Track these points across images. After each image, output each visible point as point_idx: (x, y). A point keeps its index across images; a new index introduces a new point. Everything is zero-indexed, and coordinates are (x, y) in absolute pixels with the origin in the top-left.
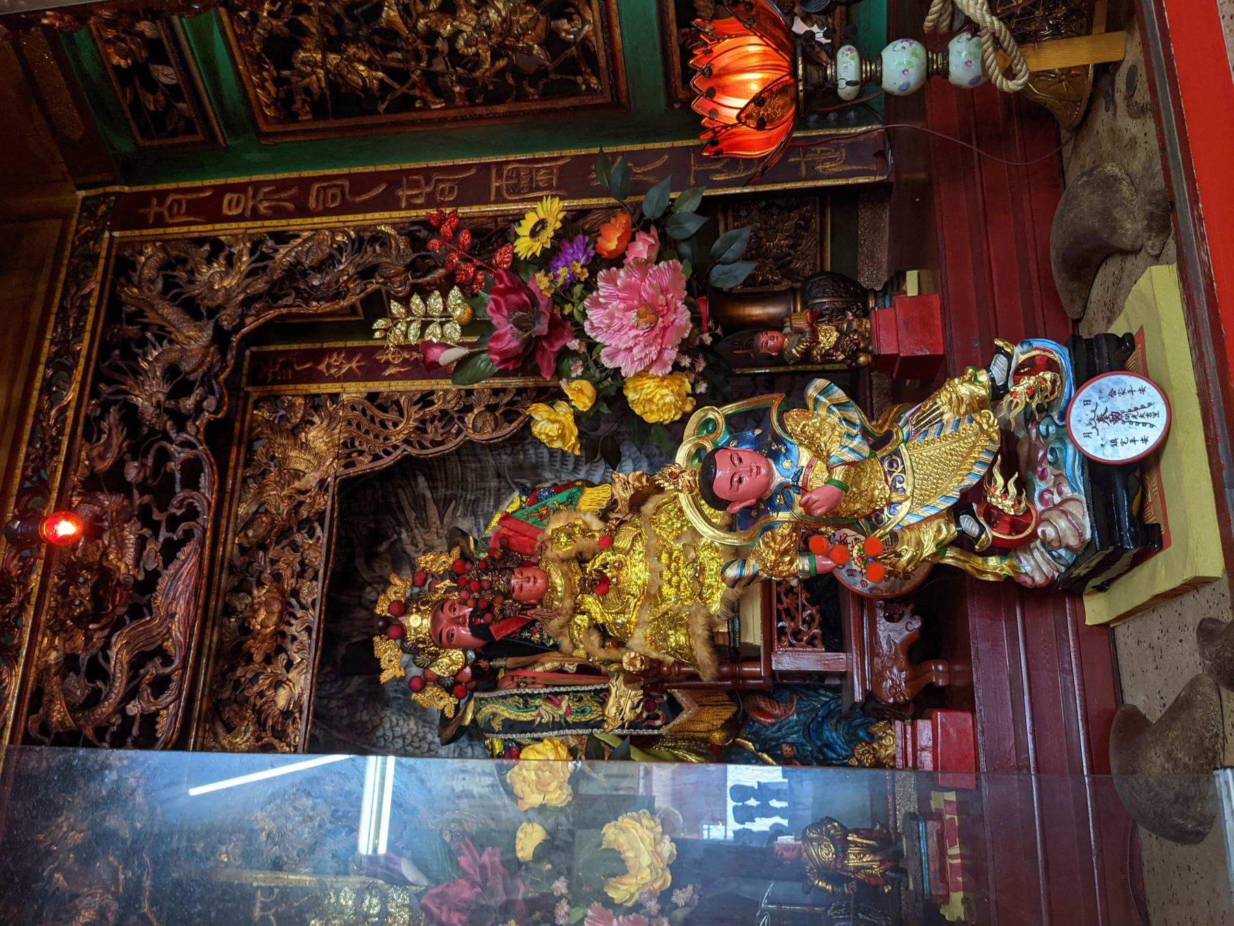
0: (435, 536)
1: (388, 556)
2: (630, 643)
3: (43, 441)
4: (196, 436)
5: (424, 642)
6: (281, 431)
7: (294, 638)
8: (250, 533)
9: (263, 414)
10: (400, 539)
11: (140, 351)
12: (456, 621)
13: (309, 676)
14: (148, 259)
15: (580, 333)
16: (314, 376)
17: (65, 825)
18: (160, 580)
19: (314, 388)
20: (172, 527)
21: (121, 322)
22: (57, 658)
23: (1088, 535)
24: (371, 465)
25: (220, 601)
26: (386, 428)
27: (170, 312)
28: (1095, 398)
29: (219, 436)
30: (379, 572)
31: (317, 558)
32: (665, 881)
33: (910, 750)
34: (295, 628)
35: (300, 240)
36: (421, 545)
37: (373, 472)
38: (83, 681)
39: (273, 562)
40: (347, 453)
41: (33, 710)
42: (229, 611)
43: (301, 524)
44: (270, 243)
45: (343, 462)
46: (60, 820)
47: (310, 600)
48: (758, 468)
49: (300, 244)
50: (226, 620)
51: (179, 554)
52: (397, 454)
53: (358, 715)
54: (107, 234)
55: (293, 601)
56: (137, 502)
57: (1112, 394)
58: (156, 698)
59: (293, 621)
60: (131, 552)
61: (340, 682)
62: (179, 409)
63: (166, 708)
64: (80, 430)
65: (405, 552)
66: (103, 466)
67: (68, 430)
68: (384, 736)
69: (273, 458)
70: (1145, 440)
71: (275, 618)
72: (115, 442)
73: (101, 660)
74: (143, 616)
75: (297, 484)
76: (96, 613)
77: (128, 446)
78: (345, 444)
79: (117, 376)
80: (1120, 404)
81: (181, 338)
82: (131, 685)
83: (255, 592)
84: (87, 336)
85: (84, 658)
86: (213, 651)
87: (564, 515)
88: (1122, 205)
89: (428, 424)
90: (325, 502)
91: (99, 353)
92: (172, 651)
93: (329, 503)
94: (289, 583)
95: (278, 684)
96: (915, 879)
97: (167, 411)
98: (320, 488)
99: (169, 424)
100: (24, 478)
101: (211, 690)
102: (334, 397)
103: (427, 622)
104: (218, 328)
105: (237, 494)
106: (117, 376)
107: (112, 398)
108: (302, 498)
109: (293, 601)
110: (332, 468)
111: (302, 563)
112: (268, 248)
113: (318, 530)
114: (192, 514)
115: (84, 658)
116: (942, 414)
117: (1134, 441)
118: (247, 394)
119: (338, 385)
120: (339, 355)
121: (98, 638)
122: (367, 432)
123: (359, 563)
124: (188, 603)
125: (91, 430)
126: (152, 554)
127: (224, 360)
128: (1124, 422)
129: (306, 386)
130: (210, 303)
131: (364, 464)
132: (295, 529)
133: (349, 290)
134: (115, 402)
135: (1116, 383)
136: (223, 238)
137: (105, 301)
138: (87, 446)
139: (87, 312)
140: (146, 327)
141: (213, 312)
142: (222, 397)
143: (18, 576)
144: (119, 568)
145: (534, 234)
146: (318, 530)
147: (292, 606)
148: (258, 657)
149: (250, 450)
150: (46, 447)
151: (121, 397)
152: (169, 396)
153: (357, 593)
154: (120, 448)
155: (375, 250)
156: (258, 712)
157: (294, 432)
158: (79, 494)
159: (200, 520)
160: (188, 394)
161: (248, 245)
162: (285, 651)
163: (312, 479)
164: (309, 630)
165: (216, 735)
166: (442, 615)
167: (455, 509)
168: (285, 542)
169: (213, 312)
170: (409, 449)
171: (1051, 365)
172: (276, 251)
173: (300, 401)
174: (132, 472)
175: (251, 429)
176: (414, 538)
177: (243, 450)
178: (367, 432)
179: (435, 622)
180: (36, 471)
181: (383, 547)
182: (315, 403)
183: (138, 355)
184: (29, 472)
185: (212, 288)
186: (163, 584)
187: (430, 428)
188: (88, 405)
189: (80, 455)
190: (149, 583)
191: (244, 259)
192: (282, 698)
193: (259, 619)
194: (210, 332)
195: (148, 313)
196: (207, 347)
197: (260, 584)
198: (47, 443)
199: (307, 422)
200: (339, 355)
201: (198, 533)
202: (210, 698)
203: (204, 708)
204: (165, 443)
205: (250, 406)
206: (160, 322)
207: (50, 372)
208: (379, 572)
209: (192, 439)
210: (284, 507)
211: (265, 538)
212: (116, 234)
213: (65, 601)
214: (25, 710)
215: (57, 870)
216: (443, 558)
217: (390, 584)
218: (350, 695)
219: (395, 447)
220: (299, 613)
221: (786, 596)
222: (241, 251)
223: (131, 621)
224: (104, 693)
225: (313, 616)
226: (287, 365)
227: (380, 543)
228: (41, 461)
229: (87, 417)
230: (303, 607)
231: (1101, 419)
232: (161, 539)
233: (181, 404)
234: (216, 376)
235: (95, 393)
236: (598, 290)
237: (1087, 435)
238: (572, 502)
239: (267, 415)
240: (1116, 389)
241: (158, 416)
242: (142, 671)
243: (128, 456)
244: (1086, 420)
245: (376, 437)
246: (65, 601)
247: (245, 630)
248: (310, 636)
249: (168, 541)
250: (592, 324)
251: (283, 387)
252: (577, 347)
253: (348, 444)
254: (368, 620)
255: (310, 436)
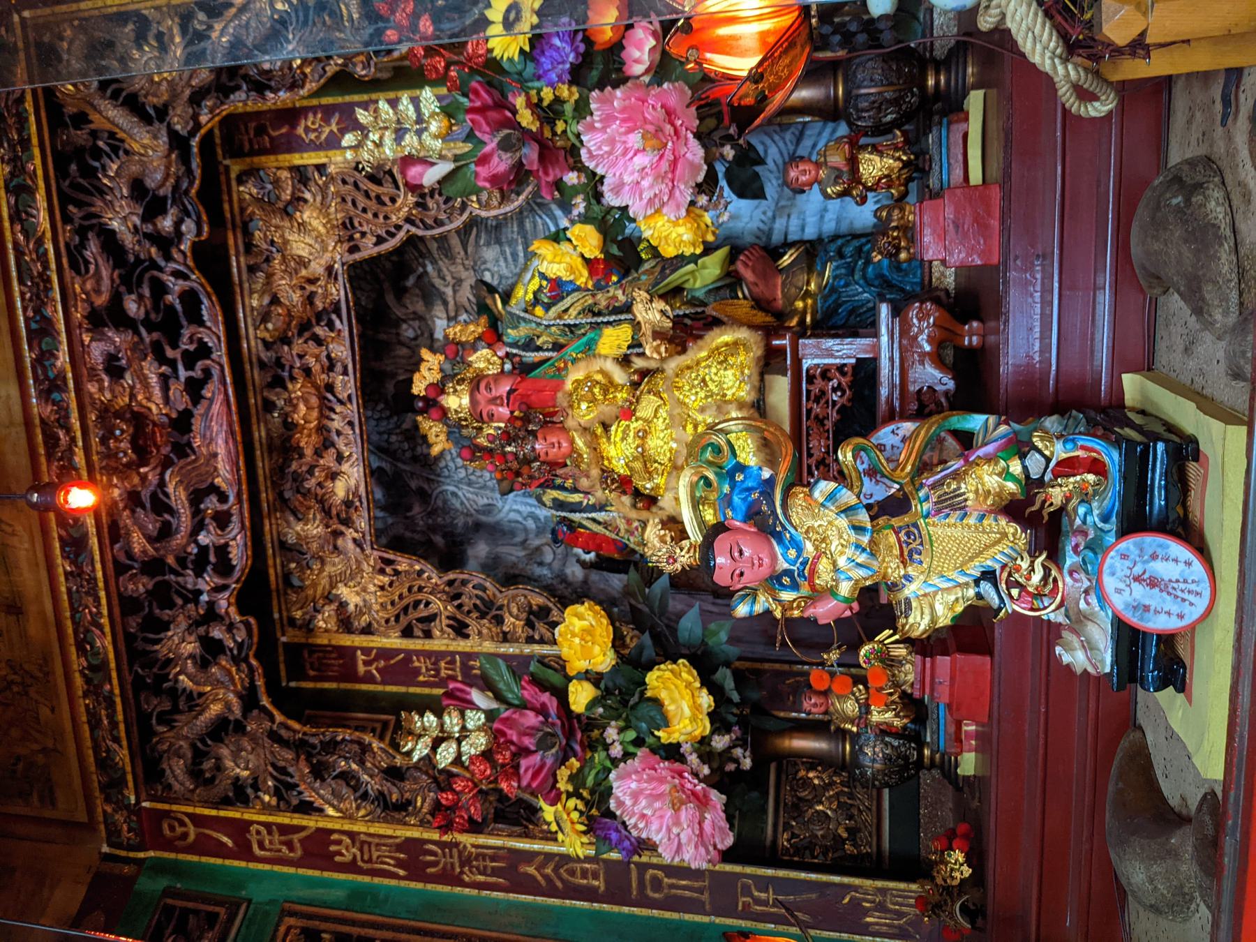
0: (461, 268)
1: (417, 291)
2: (661, 504)
3: (32, 279)
4: (185, 265)
5: (466, 420)
6: (274, 212)
7: (339, 433)
8: (270, 326)
9: (249, 190)
10: (426, 272)
11: (97, 164)
12: (493, 401)
13: (361, 469)
14: (71, 43)
15: (579, 167)
16: (293, 145)
17: (176, 638)
18: (193, 421)
19: (298, 159)
20: (189, 366)
21: (67, 126)
22: (120, 495)
23: (1108, 670)
24: (377, 249)
25: (259, 398)
26: (384, 204)
27: (113, 115)
28: (1134, 552)
29: (211, 260)
30: (411, 309)
31: (341, 351)
32: (705, 728)
33: (928, 679)
34: (337, 423)
35: (233, 10)
36: (449, 278)
37: (380, 255)
38: (152, 516)
39: (301, 357)
40: (348, 231)
41: (114, 541)
42: (269, 406)
43: (319, 316)
44: (201, 16)
45: (346, 246)
46: (170, 633)
47: (346, 395)
48: (760, 559)
49: (235, 16)
50: (269, 417)
51: (204, 392)
52: (401, 235)
53: (419, 449)
54: (16, 18)
55: (330, 396)
56: (147, 340)
57: (1154, 557)
58: (223, 529)
59: (334, 416)
60: (157, 392)
61: (395, 418)
62: (158, 232)
63: (234, 539)
64: (65, 261)
65: (433, 286)
66: (101, 300)
67: (53, 266)
68: (446, 466)
69: (272, 243)
70: (1181, 616)
71: (315, 414)
72: (105, 273)
73: (161, 496)
74: (188, 456)
75: (304, 272)
76: (142, 456)
77: (120, 276)
78: (344, 224)
79: (82, 197)
80: (1162, 569)
81: (136, 147)
82: (197, 519)
83: (290, 386)
84: (36, 152)
85: (145, 495)
86: (265, 447)
87: (582, 364)
88: (1215, 283)
89: (428, 199)
90: (338, 291)
91: (55, 169)
92: (224, 486)
93: (342, 293)
94: (322, 378)
95: (333, 476)
96: (932, 733)
97: (146, 235)
98: (330, 275)
99: (153, 250)
100: (27, 320)
101: (273, 482)
102: (321, 168)
103: (466, 401)
104: (172, 134)
105: (246, 285)
106: (82, 197)
107: (86, 223)
108: (313, 288)
109: (330, 396)
110: (337, 255)
111: (328, 357)
112: (201, 22)
113: (337, 323)
114: (204, 351)
115: (145, 495)
116: (966, 500)
117: (1169, 613)
118: (227, 168)
119: (322, 153)
120: (315, 114)
121: (153, 478)
122: (364, 210)
123: (390, 299)
124: (227, 442)
125: (77, 263)
126: (178, 393)
127: (189, 172)
128: (1161, 591)
129: (287, 156)
130: (155, 100)
131: (369, 249)
132: (314, 321)
133: (305, 75)
134: (91, 227)
135: (1160, 546)
136: (145, 12)
137: (42, 103)
138: (78, 280)
139: (27, 119)
140: (94, 134)
141: (162, 113)
142: (199, 217)
143: (58, 420)
144: (150, 409)
145: (508, 24)
146: (337, 323)
147: (329, 401)
148: (309, 452)
149: (248, 234)
150: (38, 285)
151: (94, 221)
152: (144, 219)
153: (394, 331)
154: (112, 281)
155: (324, 23)
156: (321, 501)
157: (286, 213)
158: (88, 330)
159: (214, 356)
160: (164, 212)
161: (177, 20)
162: (333, 445)
163: (317, 268)
164: (351, 424)
165: (288, 522)
166: (479, 397)
167: (478, 236)
168: (307, 335)
169: (162, 113)
170: (414, 230)
171: (1097, 467)
172: (210, 27)
173: (285, 174)
174: (132, 306)
175: (242, 210)
176: (439, 271)
177: (239, 236)
178: (364, 210)
179: (473, 401)
180: (37, 311)
181: (411, 282)
182: (301, 175)
183: (96, 169)
184: (30, 313)
185: (152, 81)
186: (197, 424)
187: (431, 203)
188: (64, 231)
189: (74, 289)
190: (183, 422)
191: (178, 39)
192: (340, 489)
193: (302, 414)
194: (165, 139)
195: (94, 116)
196: (168, 156)
197: (292, 379)
198: (37, 280)
199: (298, 200)
200: (315, 114)
201: (215, 372)
202: (273, 489)
203: (271, 498)
204: (155, 273)
205: (234, 183)
206: (108, 126)
207: (12, 201)
208: (411, 309)
209: (181, 268)
210: (296, 297)
211: (285, 331)
212: (26, 14)
213: (111, 455)
214: (107, 541)
215: (179, 673)
216: (472, 328)
217: (422, 360)
218: (407, 430)
219: (398, 227)
220: (338, 408)
221: (817, 469)
222: (170, 29)
223: (179, 458)
224: (174, 526)
225: (352, 410)
226: (261, 131)
227: (406, 277)
228: (39, 299)
229: (67, 245)
230: (341, 402)
231: (1137, 579)
232: (183, 379)
233: (159, 225)
234: (187, 192)
235: (67, 219)
236: (592, 114)
237: (1119, 591)
238: (589, 350)
239: (254, 191)
240: (1160, 552)
241: (139, 242)
242: (202, 506)
243: (122, 289)
244: (1119, 574)
245: (376, 215)
246: (111, 455)
247: (290, 426)
248: (353, 429)
249: (189, 380)
250: (590, 152)
251: (263, 159)
252: (575, 181)
253: (348, 224)
254: (411, 357)
255: (305, 216)
